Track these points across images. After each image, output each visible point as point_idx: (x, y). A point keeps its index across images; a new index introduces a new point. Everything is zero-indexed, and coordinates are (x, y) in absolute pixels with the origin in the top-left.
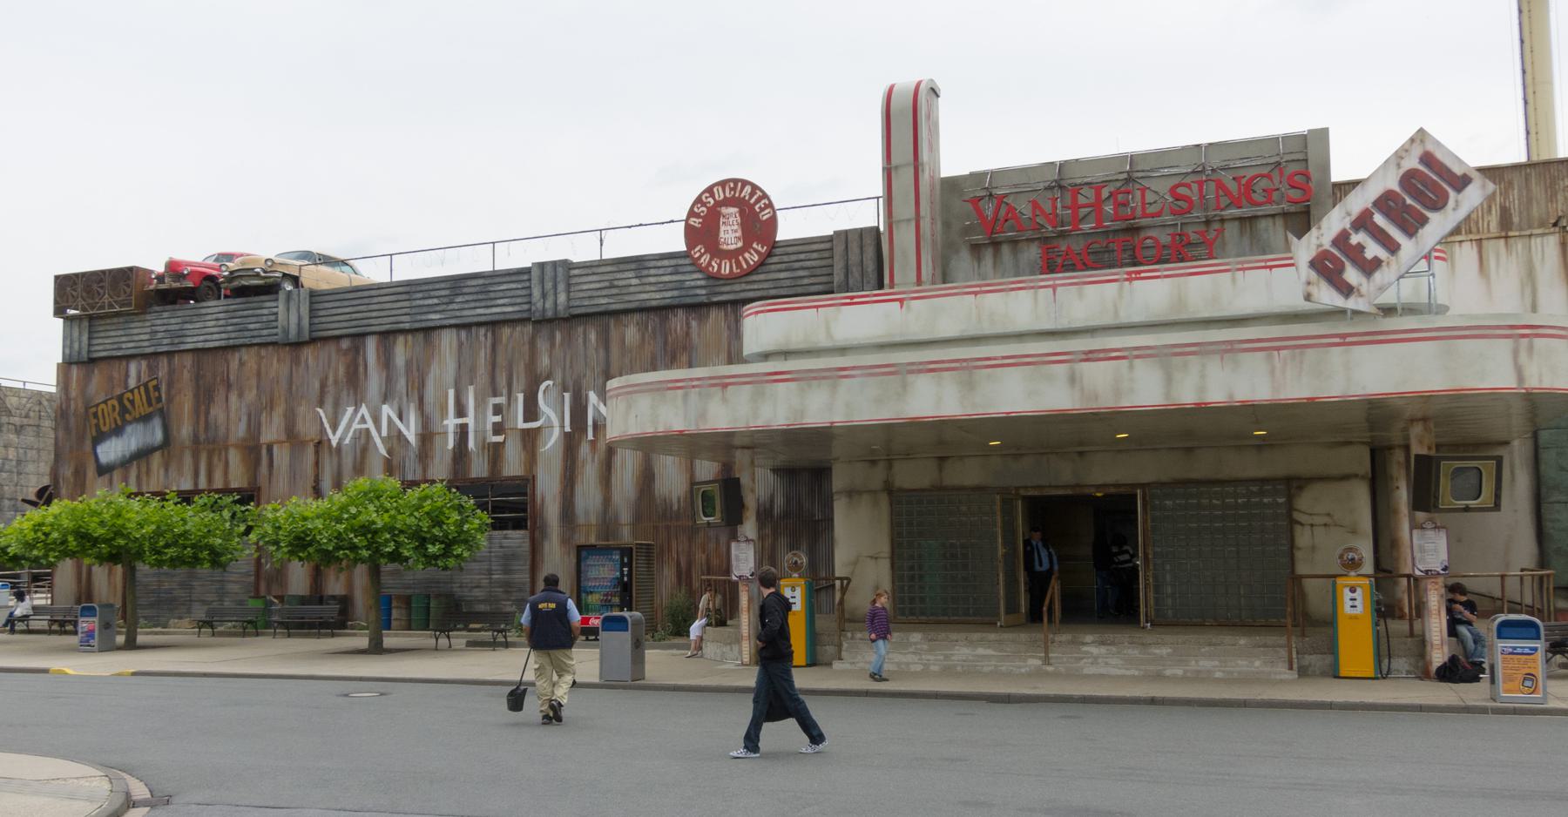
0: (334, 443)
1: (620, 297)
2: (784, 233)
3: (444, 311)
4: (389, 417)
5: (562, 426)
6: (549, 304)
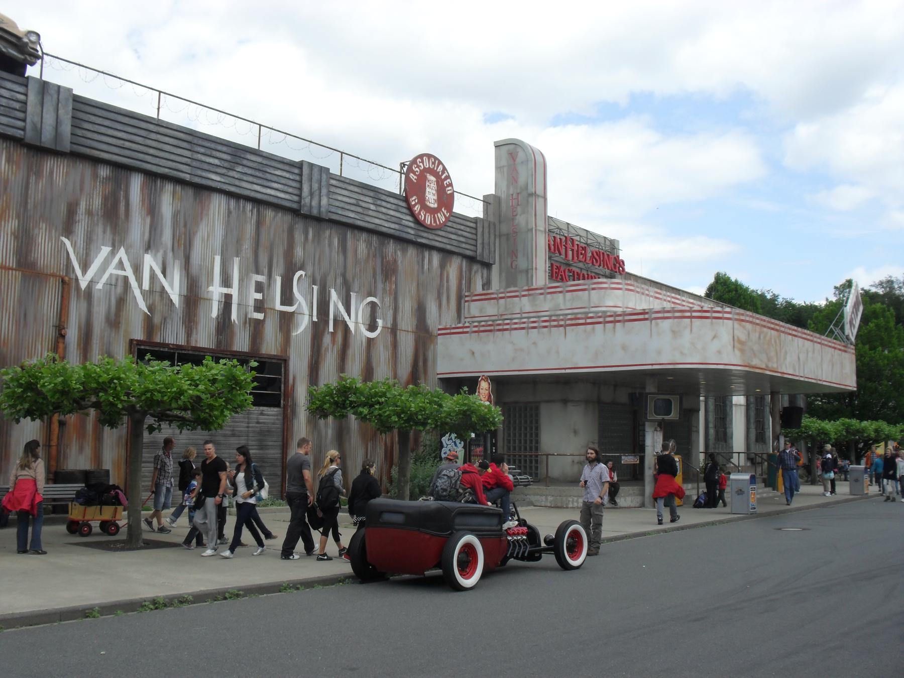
0: (83, 285)
1: (362, 216)
2: (457, 209)
3: (223, 175)
4: (152, 271)
5: (311, 315)
6: (315, 203)
